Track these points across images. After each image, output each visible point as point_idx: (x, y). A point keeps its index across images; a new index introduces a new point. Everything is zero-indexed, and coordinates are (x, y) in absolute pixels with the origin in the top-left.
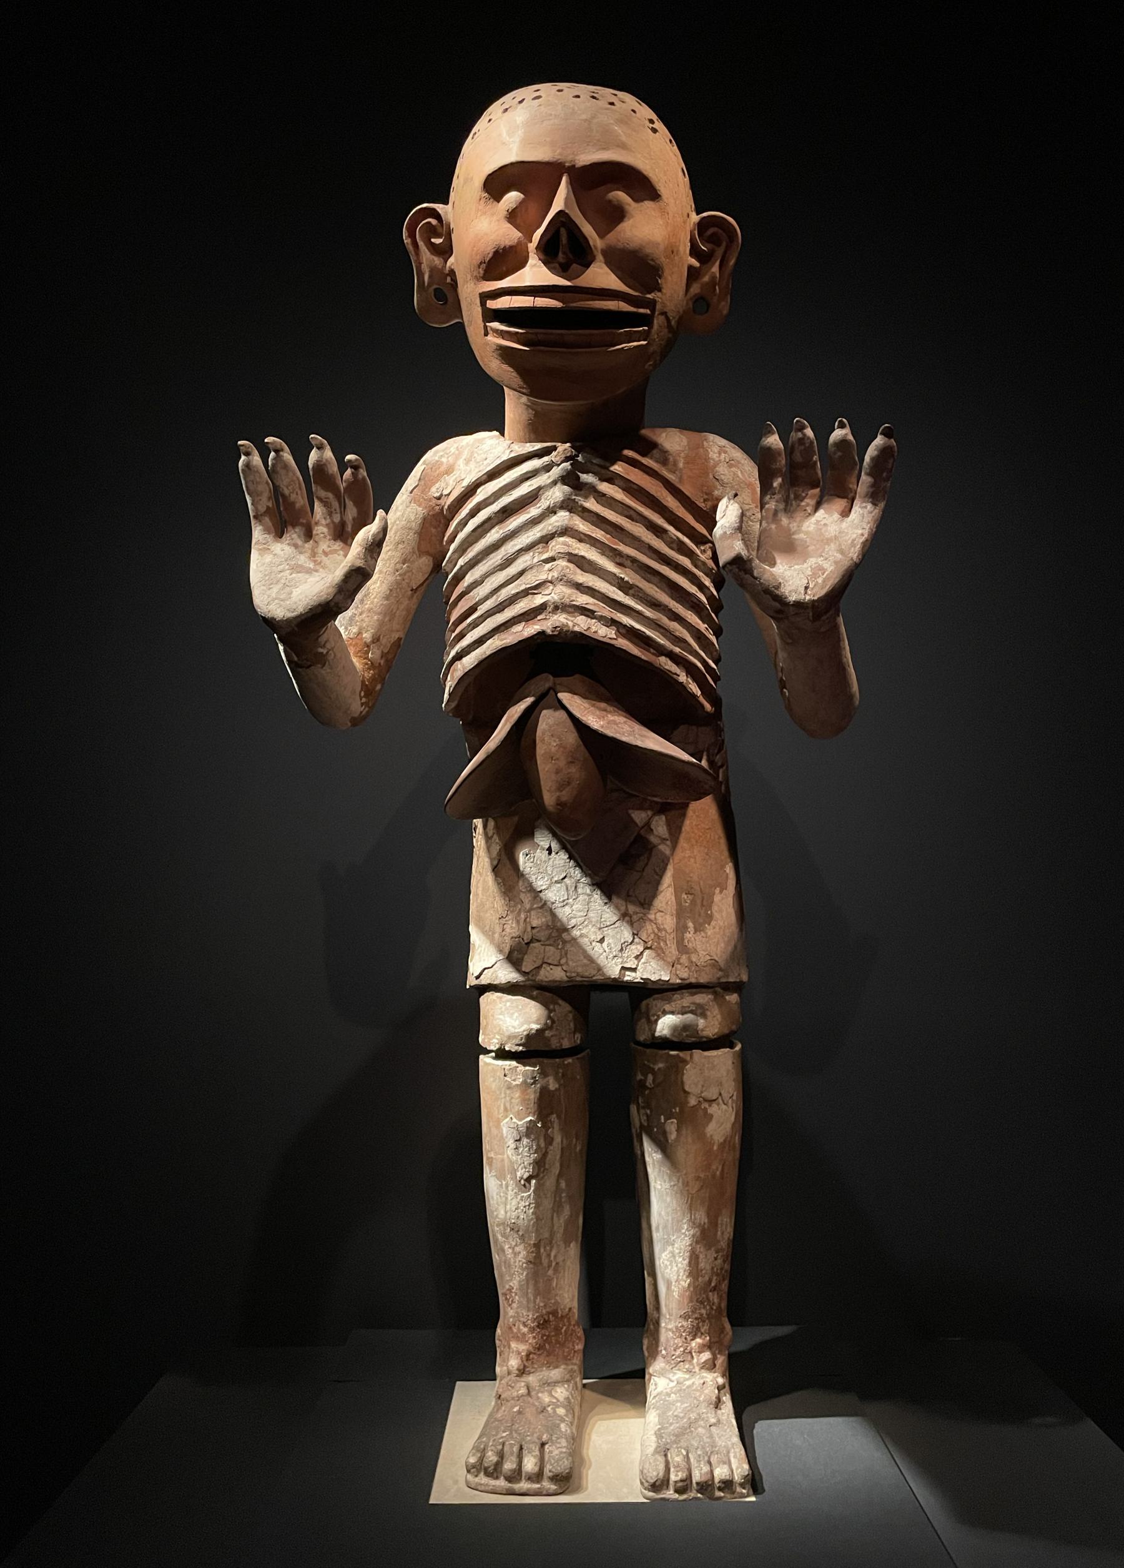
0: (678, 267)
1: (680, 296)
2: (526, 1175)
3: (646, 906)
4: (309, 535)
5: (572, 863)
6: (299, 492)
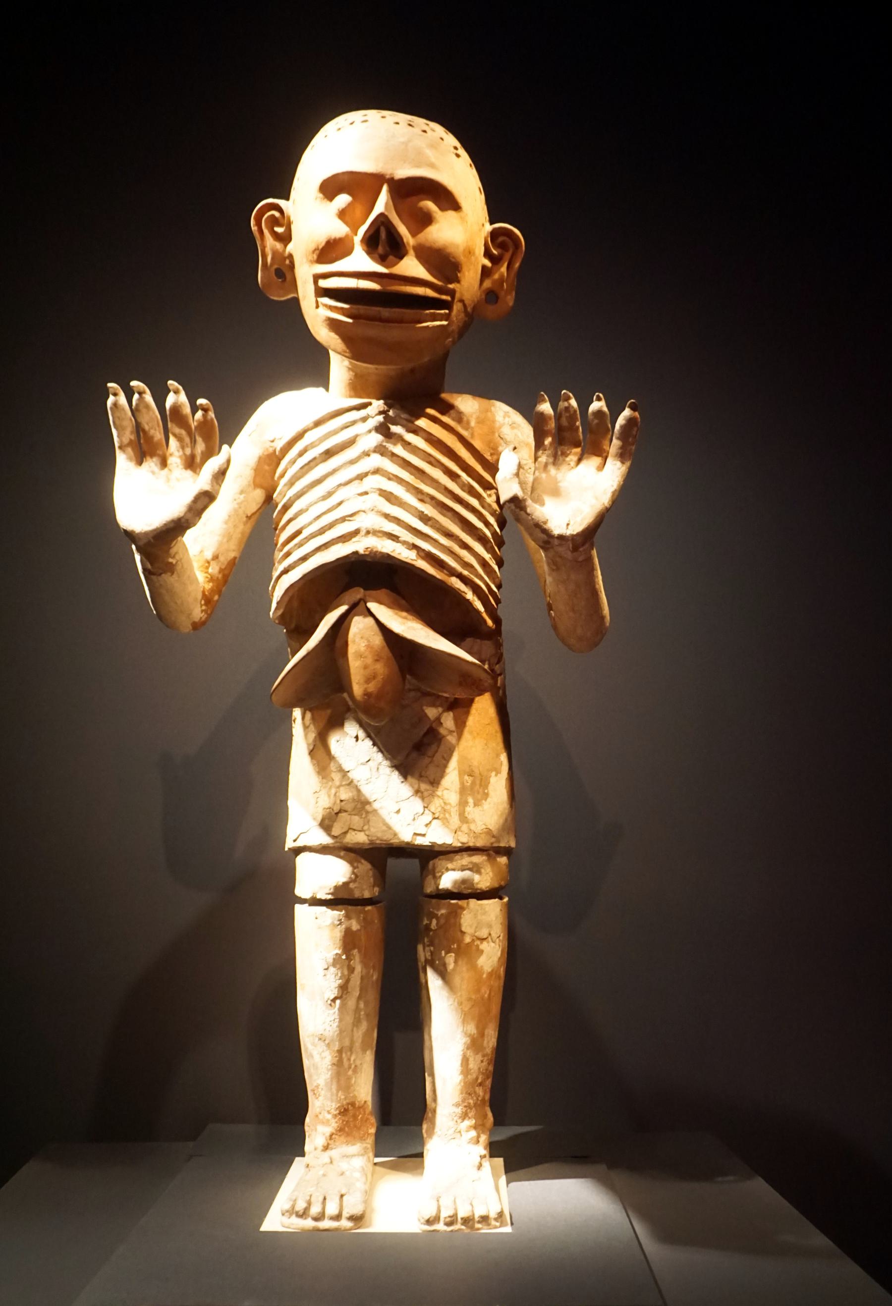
0: (474, 265)
1: (476, 288)
2: (332, 997)
3: (434, 785)
4: (164, 464)
5: (375, 749)
6: (157, 428)
